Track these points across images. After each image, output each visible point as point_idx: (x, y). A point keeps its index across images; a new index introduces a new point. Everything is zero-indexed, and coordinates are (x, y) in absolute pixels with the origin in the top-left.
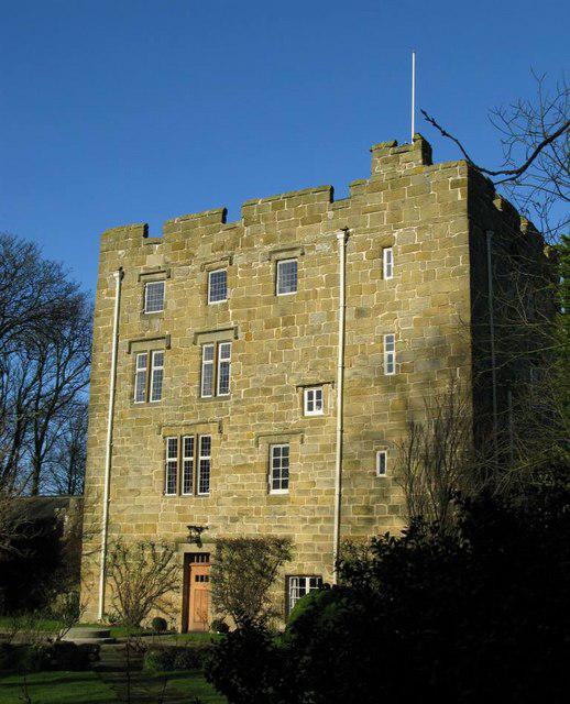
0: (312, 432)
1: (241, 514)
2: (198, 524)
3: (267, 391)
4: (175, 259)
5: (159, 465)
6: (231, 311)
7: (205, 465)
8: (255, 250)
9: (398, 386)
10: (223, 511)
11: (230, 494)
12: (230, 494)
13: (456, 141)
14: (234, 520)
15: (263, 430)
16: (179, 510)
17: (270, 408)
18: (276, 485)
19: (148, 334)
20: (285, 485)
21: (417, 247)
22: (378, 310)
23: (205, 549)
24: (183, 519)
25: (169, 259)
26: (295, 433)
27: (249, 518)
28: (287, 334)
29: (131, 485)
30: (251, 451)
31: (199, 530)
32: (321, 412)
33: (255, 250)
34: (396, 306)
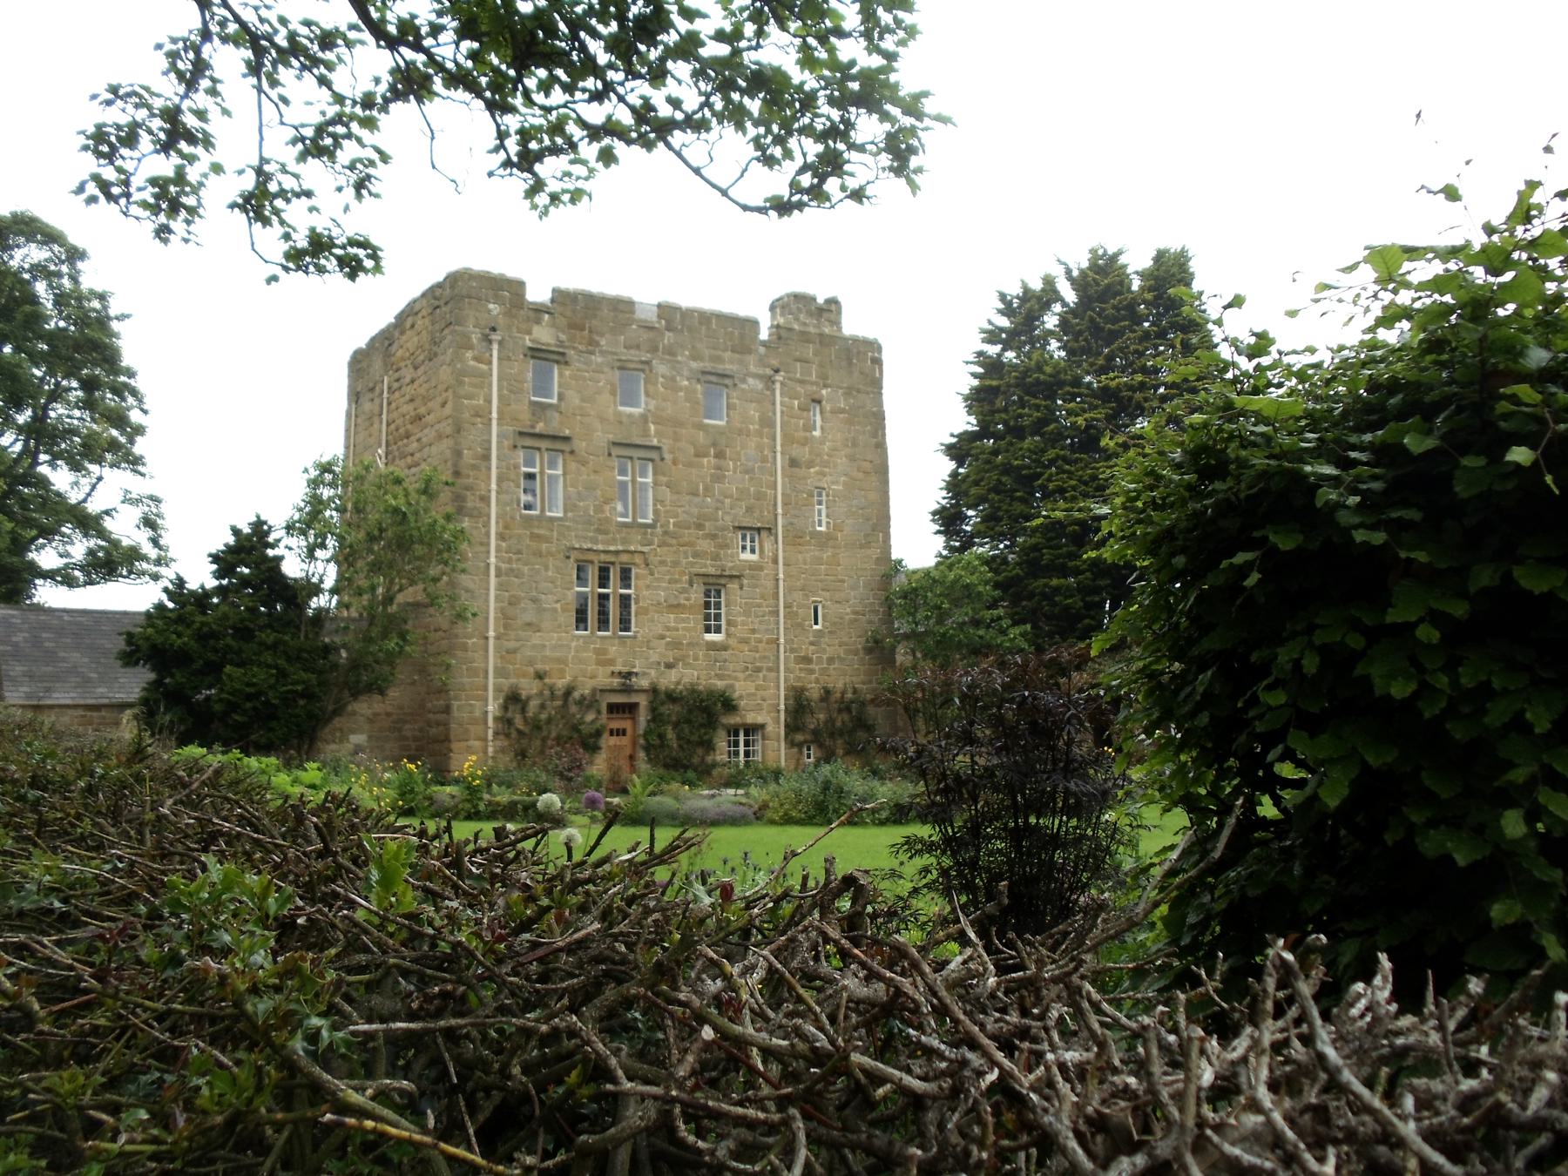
0: (753, 577)
1: (677, 660)
2: (625, 669)
3: (700, 526)
4: (572, 339)
5: (64, 589)
6: (652, 427)
7: (625, 601)
8: (1108, 456)
9: (831, 543)
10: (654, 657)
11: (662, 637)
12: (662, 637)
13: (262, 139)
14: (669, 666)
15: (696, 570)
16: (598, 652)
17: (705, 545)
18: (708, 630)
19: (540, 427)
20: (718, 630)
21: (842, 411)
22: (810, 464)
23: (634, 699)
24: (600, 663)
25: (563, 337)
26: (731, 577)
27: (686, 665)
28: (718, 468)
29: (528, 617)
30: (684, 591)
31: (629, 675)
32: (755, 557)
33: (1108, 456)
34: (826, 464)
